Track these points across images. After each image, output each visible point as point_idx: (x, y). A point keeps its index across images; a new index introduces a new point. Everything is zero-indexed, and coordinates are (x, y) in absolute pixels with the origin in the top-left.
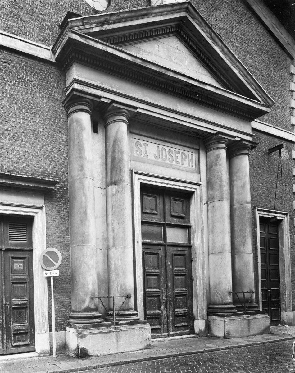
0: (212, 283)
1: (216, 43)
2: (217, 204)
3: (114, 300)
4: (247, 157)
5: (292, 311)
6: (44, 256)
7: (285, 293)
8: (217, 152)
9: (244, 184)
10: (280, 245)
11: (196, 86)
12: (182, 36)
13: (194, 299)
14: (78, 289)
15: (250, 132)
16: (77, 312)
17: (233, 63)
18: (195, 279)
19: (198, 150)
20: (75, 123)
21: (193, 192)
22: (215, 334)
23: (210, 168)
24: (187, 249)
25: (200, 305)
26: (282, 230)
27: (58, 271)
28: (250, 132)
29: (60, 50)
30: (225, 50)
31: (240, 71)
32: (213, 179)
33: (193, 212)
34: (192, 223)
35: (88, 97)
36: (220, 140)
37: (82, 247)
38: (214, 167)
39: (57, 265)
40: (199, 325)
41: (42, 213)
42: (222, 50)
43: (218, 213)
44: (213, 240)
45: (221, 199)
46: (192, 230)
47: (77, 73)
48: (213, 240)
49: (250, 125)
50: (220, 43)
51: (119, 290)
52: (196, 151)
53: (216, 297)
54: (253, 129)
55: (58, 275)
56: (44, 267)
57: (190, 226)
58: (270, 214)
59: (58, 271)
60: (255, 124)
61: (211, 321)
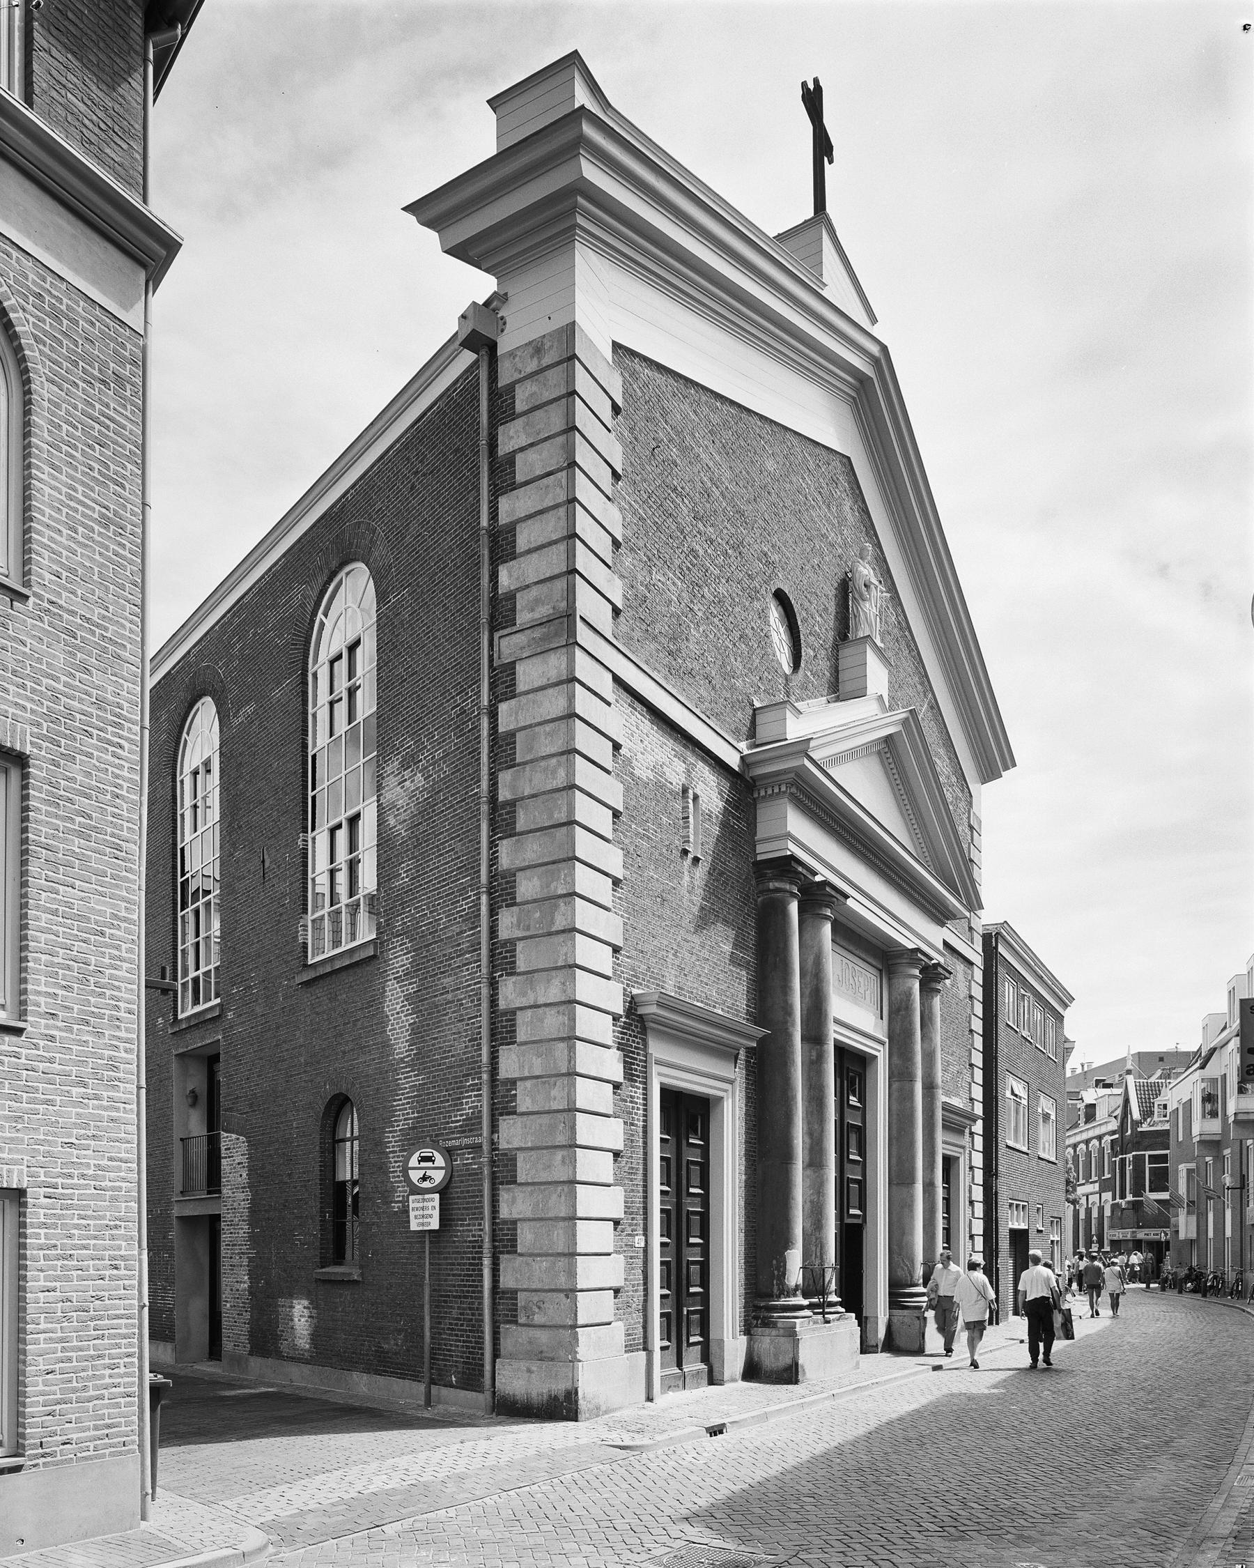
19: (880, 971)
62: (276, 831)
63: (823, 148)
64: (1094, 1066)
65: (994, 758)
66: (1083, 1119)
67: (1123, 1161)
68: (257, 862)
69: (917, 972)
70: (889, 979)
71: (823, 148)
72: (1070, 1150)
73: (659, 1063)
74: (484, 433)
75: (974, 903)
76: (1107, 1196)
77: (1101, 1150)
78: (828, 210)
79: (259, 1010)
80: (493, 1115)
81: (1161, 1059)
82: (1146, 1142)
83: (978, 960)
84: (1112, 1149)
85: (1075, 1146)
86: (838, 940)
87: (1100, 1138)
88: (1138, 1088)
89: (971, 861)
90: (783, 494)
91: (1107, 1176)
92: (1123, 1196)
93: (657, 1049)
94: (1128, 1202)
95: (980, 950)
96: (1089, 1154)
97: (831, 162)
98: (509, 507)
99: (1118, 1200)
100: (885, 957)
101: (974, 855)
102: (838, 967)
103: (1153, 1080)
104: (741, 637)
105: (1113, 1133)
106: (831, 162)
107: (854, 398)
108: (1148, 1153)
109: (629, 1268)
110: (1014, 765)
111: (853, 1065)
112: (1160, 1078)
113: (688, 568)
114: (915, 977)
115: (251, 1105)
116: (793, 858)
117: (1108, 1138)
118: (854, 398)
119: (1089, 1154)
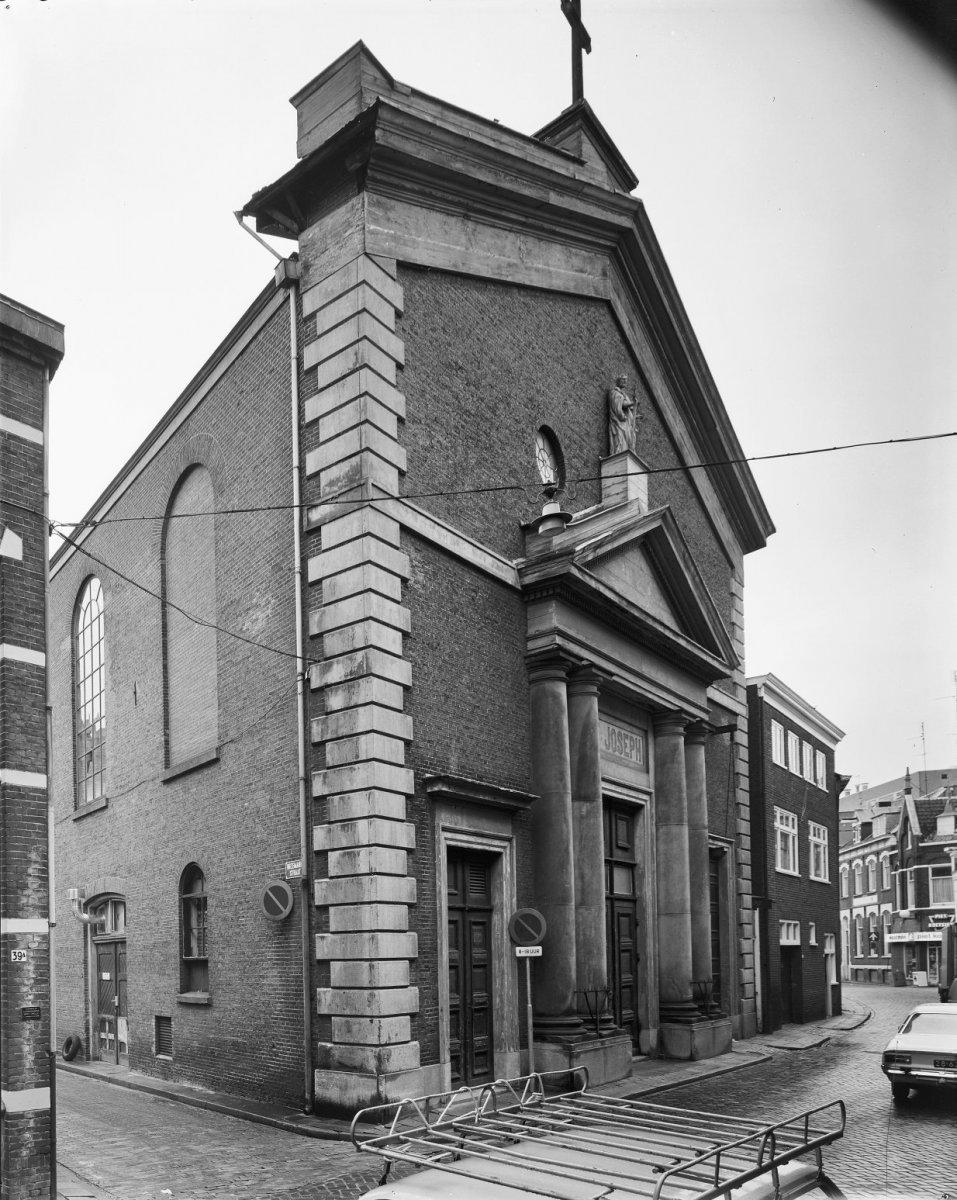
0: (664, 966)
1: (688, 568)
2: (674, 829)
3: (371, 967)
4: (703, 748)
5: (829, 1029)
6: (517, 922)
7: (728, 981)
8: (673, 740)
9: (701, 795)
10: (721, 896)
11: (669, 638)
12: (647, 549)
13: (639, 994)
14: (554, 978)
15: (704, 704)
16: (552, 1016)
17: (702, 599)
18: (641, 957)
19: (646, 732)
20: (550, 699)
21: (642, 806)
22: (673, 1053)
23: (661, 765)
24: (631, 905)
25: (650, 1003)
26: (726, 869)
27: (540, 948)
28: (704, 704)
29: (539, 576)
30: (697, 579)
31: (709, 612)
32: (668, 786)
33: (640, 840)
34: (638, 859)
35: (572, 659)
36: (679, 721)
37: (562, 907)
38: (669, 765)
39: (539, 938)
40: (650, 1037)
41: (511, 848)
42: (693, 579)
43: (675, 844)
44: (667, 891)
45: (680, 823)
46: (638, 872)
47: (554, 618)
48: (667, 891)
49: (705, 692)
50: (692, 569)
51: (592, 979)
52: (642, 733)
53: (670, 991)
54: (710, 700)
55: (540, 954)
56: (516, 938)
57: (635, 865)
58: (716, 843)
59: (540, 948)
60: (713, 693)
61: (666, 1032)
62: (144, 669)
63: (581, 41)
64: (869, 787)
65: (753, 529)
66: (858, 837)
67: (903, 875)
68: (131, 692)
69: (681, 730)
70: (655, 737)
71: (581, 41)
72: (846, 866)
73: (445, 829)
74: (294, 353)
75: (734, 663)
76: (888, 907)
77: (880, 866)
78: (585, 96)
79: (133, 801)
80: (307, 823)
81: (944, 777)
82: (929, 856)
83: (742, 710)
84: (891, 863)
85: (850, 862)
86: (605, 710)
87: (877, 853)
88: (918, 805)
89: (733, 624)
90: (545, 346)
91: (887, 887)
92: (904, 906)
93: (444, 819)
94: (911, 912)
95: (744, 701)
96: (866, 869)
97: (589, 51)
98: (314, 407)
99: (898, 910)
100: (651, 718)
101: (735, 618)
102: (604, 733)
103: (936, 797)
104: (511, 471)
105: (893, 848)
106: (589, 51)
107: (614, 250)
108: (930, 867)
109: (480, 960)
110: (774, 531)
111: (622, 812)
112: (944, 794)
113: (463, 427)
114: (680, 734)
115: (129, 872)
116: (560, 648)
117: (886, 853)
118: (614, 250)
119: (866, 869)
